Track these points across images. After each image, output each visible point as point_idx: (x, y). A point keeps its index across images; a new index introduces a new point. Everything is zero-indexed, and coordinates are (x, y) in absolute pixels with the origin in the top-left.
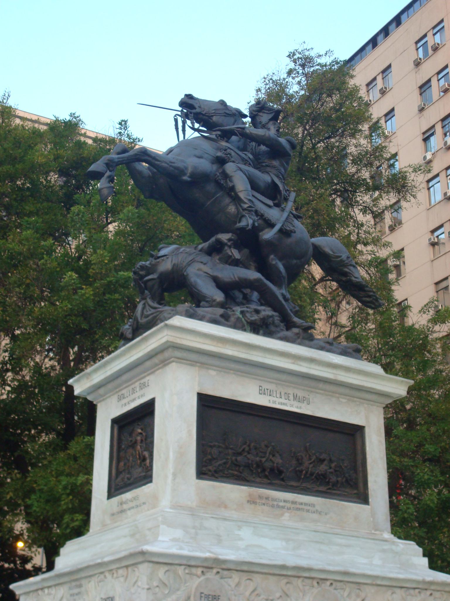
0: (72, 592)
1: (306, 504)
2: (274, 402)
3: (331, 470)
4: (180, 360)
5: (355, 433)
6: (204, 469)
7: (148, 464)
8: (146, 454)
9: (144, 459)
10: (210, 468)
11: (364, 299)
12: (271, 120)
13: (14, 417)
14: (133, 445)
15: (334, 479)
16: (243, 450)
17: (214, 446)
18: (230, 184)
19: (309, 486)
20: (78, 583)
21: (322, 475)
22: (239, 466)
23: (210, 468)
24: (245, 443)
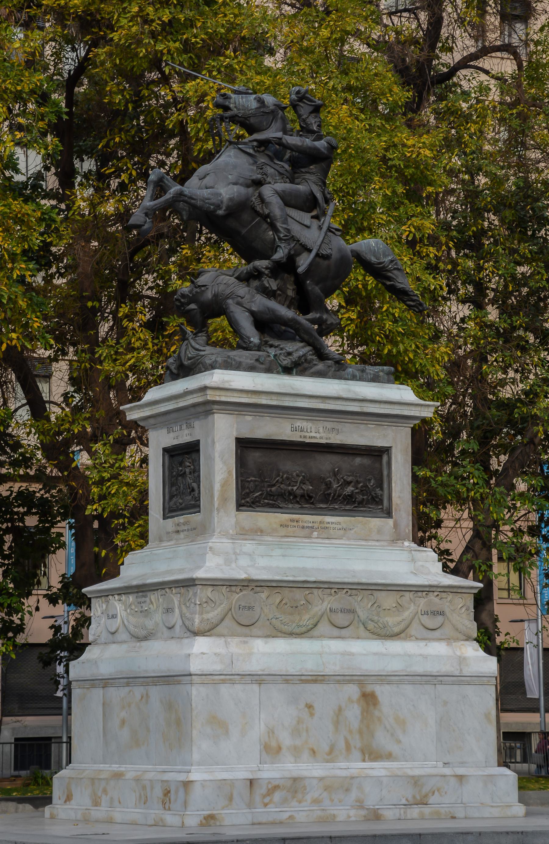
0: (139, 600)
1: (332, 523)
2: (305, 437)
3: (357, 491)
4: (220, 411)
5: (379, 454)
6: (243, 501)
7: (196, 495)
8: (195, 485)
9: (193, 490)
10: (248, 500)
11: (408, 303)
12: (311, 113)
13: (62, 262)
14: (184, 475)
15: (360, 497)
16: (277, 481)
17: (251, 481)
18: (267, 211)
19: (336, 507)
20: (144, 594)
21: (348, 495)
22: (274, 496)
23: (248, 500)
24: (279, 475)
